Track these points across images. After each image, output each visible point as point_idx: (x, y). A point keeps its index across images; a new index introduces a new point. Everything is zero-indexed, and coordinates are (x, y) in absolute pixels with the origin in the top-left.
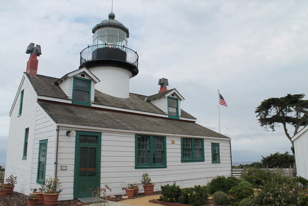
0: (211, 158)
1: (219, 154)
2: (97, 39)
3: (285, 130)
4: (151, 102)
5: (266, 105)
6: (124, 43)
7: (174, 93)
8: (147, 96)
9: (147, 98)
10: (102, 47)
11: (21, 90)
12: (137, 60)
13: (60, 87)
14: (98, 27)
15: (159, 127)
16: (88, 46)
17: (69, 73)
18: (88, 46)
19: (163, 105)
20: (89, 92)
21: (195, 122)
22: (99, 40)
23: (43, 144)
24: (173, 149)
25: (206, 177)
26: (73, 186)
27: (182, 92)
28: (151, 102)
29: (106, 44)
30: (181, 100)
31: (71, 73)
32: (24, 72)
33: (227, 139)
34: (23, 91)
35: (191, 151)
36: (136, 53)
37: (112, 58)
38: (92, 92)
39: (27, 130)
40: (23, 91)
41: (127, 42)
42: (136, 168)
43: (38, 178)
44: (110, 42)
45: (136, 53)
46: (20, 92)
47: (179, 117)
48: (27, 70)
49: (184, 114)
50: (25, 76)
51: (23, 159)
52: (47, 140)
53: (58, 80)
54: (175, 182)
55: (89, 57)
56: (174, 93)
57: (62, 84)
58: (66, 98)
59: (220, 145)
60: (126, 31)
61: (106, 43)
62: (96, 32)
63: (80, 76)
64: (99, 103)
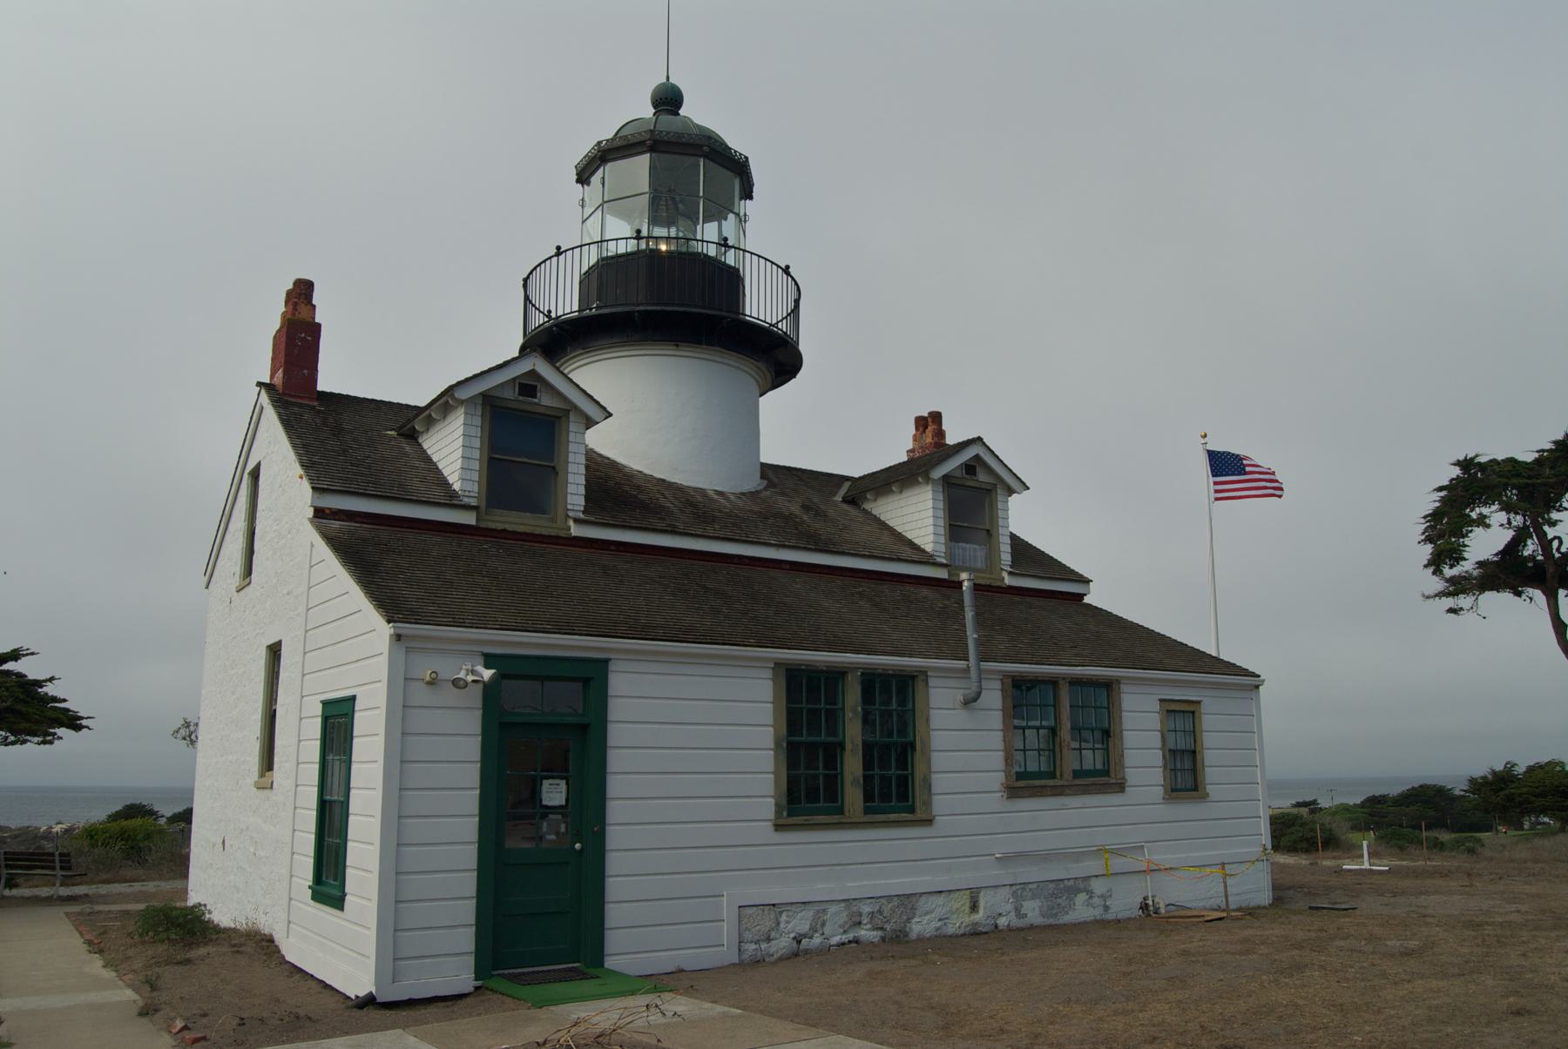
0: (1157, 776)
1: (345, 804)
2: (599, 212)
3: (1555, 627)
4: (867, 506)
5: (1476, 483)
6: (729, 226)
7: (977, 457)
8: (847, 478)
9: (847, 485)
10: (622, 250)
11: (248, 469)
12: (797, 302)
13: (425, 446)
14: (604, 154)
15: (907, 632)
16: (558, 248)
17: (459, 383)
18: (558, 248)
19: (917, 517)
20: (552, 472)
21: (1081, 596)
22: (608, 218)
23: (337, 720)
24: (963, 736)
25: (953, 895)
26: (470, 945)
27: (1010, 452)
28: (867, 506)
29: (638, 236)
30: (1011, 491)
31: (597, 403)
32: (260, 384)
33: (1242, 680)
34: (258, 467)
35: (1063, 742)
36: (788, 274)
37: (679, 304)
38: (571, 468)
39: (275, 651)
40: (258, 467)
41: (742, 220)
42: (778, 827)
43: (318, 879)
44: (661, 225)
45: (788, 274)
46: (246, 475)
47: (1005, 575)
48: (272, 377)
49: (1026, 555)
50: (265, 399)
51: (260, 788)
52: (353, 698)
53: (417, 415)
54: (908, 901)
55: (565, 301)
56: (977, 457)
57: (432, 431)
58: (450, 499)
59: (1204, 708)
60: (738, 168)
61: (639, 231)
62: (596, 179)
63: (510, 394)
64: (660, 525)
